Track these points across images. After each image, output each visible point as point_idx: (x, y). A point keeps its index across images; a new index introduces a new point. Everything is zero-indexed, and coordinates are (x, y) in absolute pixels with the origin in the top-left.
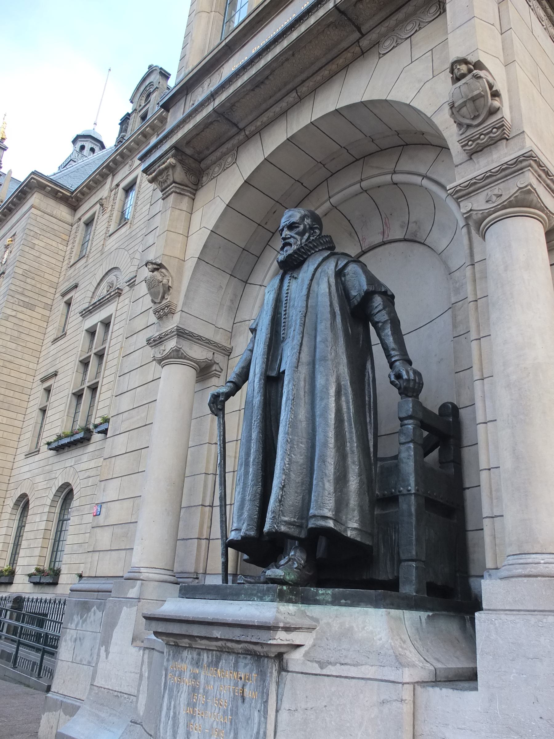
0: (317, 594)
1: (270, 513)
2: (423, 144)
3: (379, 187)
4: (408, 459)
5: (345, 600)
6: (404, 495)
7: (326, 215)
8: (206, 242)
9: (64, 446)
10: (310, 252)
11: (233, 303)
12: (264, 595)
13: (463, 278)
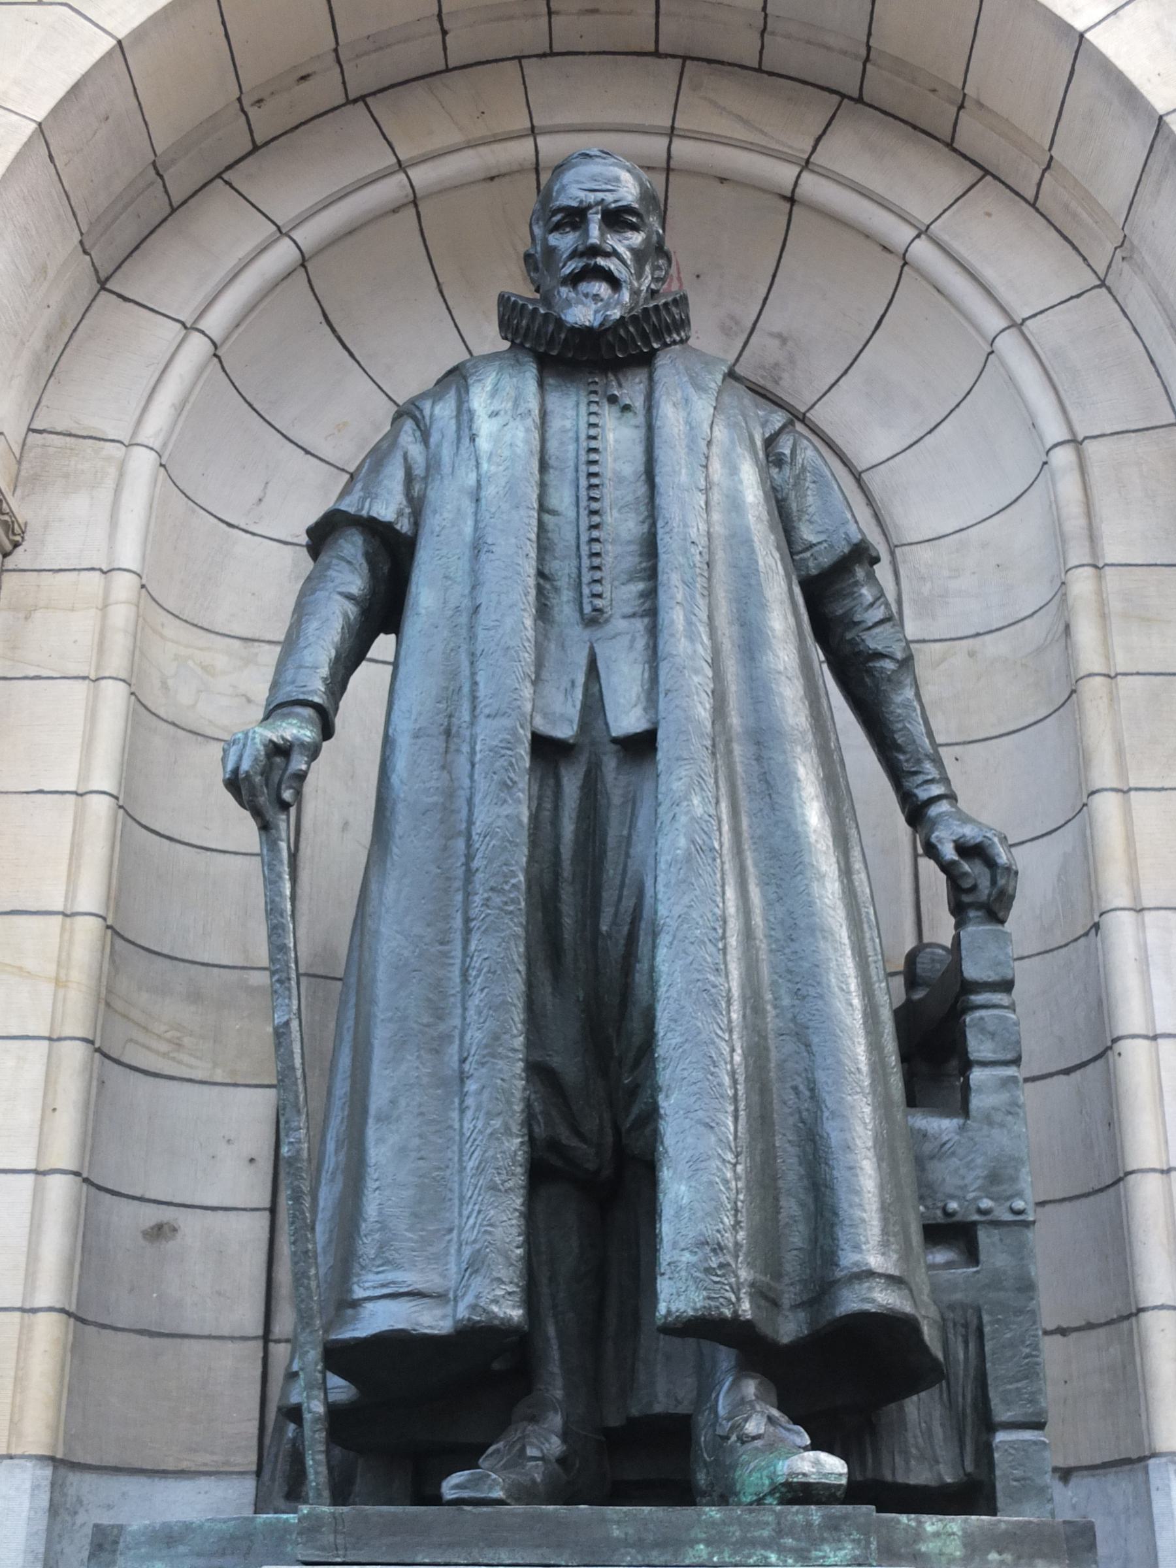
0: (918, 1535)
1: (286, 1226)
2: (915, 127)
3: (723, 180)
4: (1010, 1113)
5: (1000, 1553)
6: (997, 1224)
7: (492, 179)
8: (86, 76)
9: (492, 889)
10: (670, 334)
11: (47, 350)
12: (817, 1542)
13: (946, 573)
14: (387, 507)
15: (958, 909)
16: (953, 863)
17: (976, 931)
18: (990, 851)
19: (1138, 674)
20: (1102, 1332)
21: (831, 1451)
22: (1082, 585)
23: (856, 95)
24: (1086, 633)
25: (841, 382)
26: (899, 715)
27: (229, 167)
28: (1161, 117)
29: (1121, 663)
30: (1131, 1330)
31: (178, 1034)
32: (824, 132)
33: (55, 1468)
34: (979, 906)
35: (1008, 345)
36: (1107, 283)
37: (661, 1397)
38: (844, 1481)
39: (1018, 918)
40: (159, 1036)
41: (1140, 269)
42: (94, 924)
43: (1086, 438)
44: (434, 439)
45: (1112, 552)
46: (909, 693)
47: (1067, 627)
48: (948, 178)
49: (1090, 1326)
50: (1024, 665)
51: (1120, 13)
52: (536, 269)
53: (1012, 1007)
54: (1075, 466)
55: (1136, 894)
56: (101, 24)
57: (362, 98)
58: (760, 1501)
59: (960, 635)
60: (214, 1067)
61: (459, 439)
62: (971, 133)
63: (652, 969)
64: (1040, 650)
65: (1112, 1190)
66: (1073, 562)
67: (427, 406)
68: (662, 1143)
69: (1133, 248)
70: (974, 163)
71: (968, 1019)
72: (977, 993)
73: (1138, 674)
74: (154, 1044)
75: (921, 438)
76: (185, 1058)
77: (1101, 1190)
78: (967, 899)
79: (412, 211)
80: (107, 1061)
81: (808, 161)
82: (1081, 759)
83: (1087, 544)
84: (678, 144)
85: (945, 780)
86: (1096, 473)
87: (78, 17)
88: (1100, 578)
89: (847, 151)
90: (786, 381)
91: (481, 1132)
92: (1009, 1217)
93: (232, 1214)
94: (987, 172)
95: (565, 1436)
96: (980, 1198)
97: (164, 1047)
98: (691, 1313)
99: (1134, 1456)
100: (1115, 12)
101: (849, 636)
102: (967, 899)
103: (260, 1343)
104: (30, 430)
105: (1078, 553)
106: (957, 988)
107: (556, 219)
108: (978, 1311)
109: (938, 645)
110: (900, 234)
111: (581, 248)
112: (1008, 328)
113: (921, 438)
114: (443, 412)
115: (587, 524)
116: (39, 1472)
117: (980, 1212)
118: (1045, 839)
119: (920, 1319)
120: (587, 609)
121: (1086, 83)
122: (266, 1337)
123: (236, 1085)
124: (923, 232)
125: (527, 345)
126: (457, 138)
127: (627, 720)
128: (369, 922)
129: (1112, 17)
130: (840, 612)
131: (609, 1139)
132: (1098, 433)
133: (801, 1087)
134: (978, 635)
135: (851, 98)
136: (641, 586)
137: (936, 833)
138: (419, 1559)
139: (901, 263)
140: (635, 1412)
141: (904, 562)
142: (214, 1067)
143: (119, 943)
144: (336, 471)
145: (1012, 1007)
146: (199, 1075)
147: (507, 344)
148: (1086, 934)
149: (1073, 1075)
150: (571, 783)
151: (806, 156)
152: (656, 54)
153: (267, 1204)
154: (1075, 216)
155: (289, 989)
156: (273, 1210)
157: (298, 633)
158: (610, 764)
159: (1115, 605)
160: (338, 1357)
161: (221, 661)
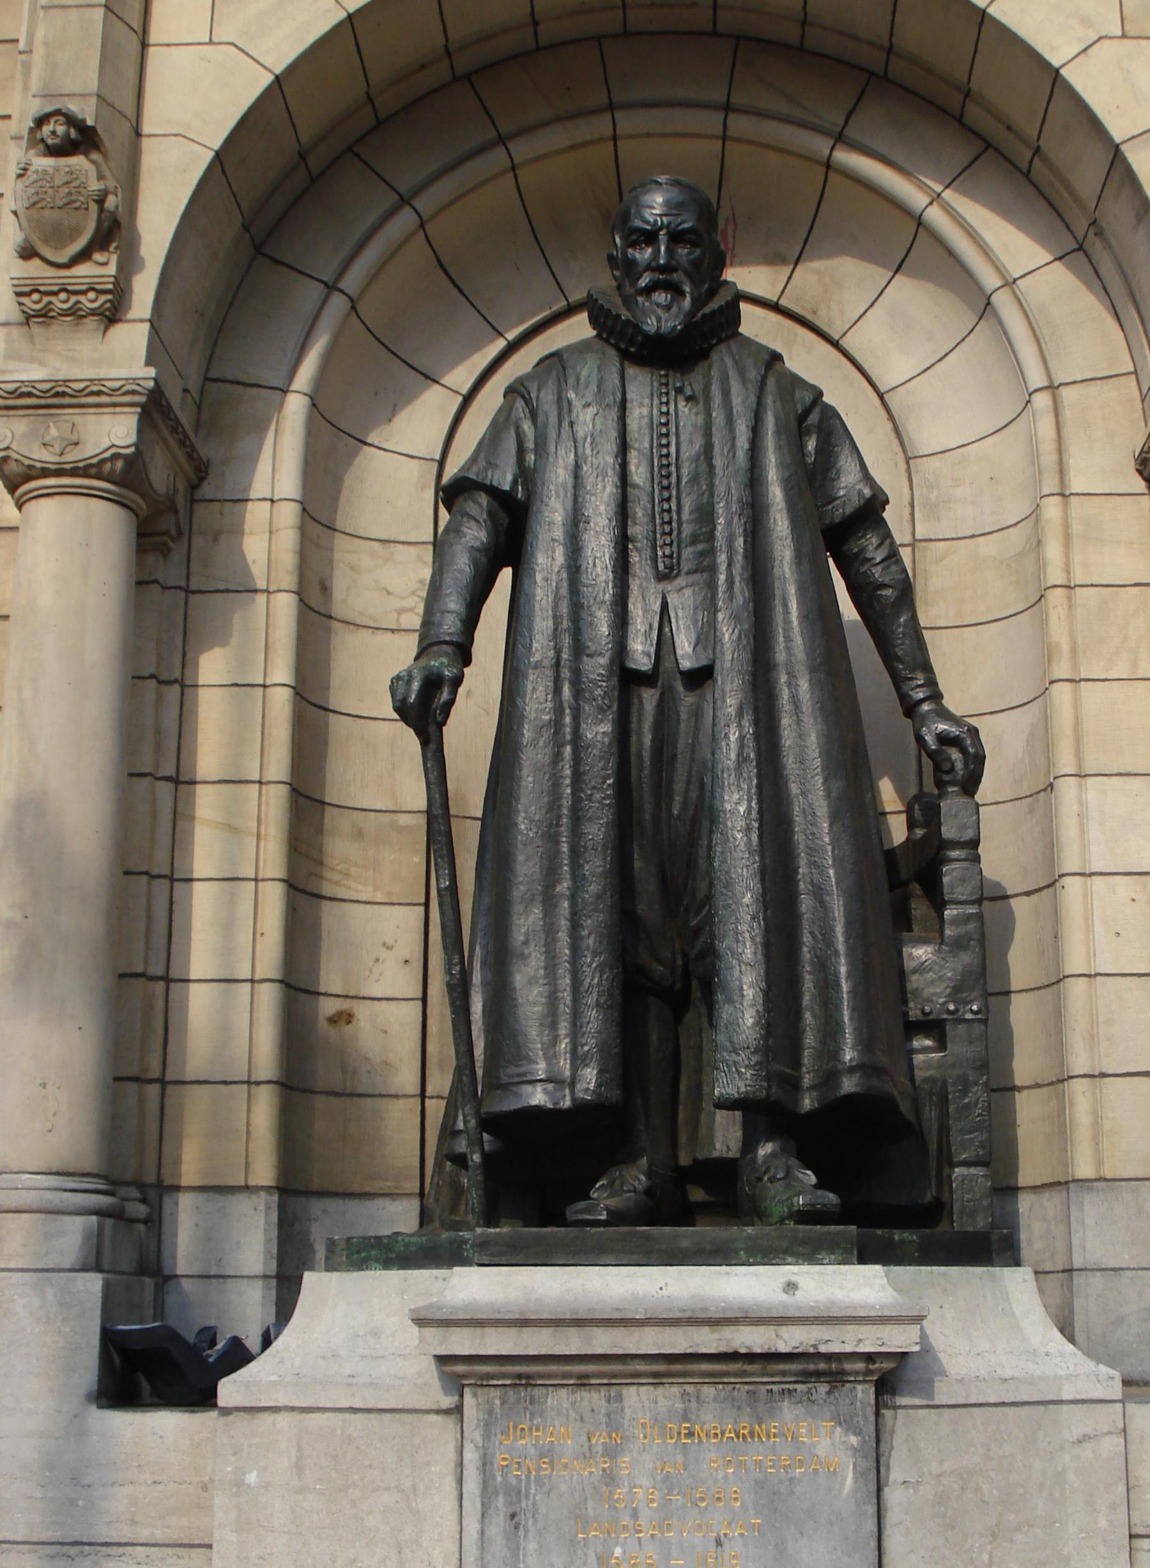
14: (504, 479)
19: (1092, 585)
20: (1045, 1089)
21: (831, 1191)
22: (1052, 509)
23: (882, 73)
24: (1053, 551)
25: (868, 313)
27: (358, 141)
28: (1117, 146)
29: (1079, 578)
30: (1064, 1091)
32: (855, 107)
33: (280, 1195)
36: (1086, 246)
37: (718, 1146)
38: (838, 1210)
39: (986, 790)
41: (1108, 245)
42: (283, 790)
43: (1060, 385)
44: (541, 418)
45: (1077, 484)
47: (1039, 542)
49: (1038, 1086)
50: (1009, 566)
51: (1089, 51)
54: (1051, 409)
55: (1080, 764)
56: (261, 61)
57: (467, 77)
58: (782, 1221)
59: (959, 535)
61: (560, 425)
62: (974, 114)
63: (710, 847)
64: (1021, 555)
65: (1055, 987)
66: (1046, 491)
67: (533, 388)
70: (978, 136)
72: (954, 849)
73: (1092, 585)
75: (933, 365)
77: (1048, 986)
78: (946, 778)
79: (511, 174)
80: (297, 893)
81: (841, 134)
82: (1048, 654)
83: (1057, 476)
84: (733, 118)
86: (1068, 413)
87: (242, 55)
88: (1066, 506)
90: (823, 313)
93: (394, 1003)
95: (649, 1174)
98: (736, 1096)
99: (1063, 1180)
100: (1085, 50)
101: (863, 570)
102: (946, 778)
103: (419, 1100)
104: (207, 379)
105: (1050, 484)
107: (634, 237)
108: (944, 1082)
109: (942, 544)
111: (654, 264)
112: (1002, 287)
113: (933, 365)
114: (546, 398)
116: (269, 1198)
117: (949, 1012)
118: (1019, 709)
119: (898, 1098)
120: (661, 567)
121: (1059, 106)
122: (423, 1095)
123: (392, 904)
125: (612, 341)
129: (1083, 55)
131: (679, 962)
132: (1071, 380)
134: (973, 536)
135: (878, 76)
138: (553, 1262)
140: (700, 1156)
141: (917, 472)
143: (302, 800)
144: (451, 393)
146: (364, 897)
147: (595, 333)
148: (1045, 790)
149: (1032, 897)
150: (649, 698)
151: (839, 130)
152: (714, 33)
153: (420, 995)
156: (424, 1000)
157: (441, 579)
158: (680, 687)
159: (1077, 528)
160: (490, 1123)
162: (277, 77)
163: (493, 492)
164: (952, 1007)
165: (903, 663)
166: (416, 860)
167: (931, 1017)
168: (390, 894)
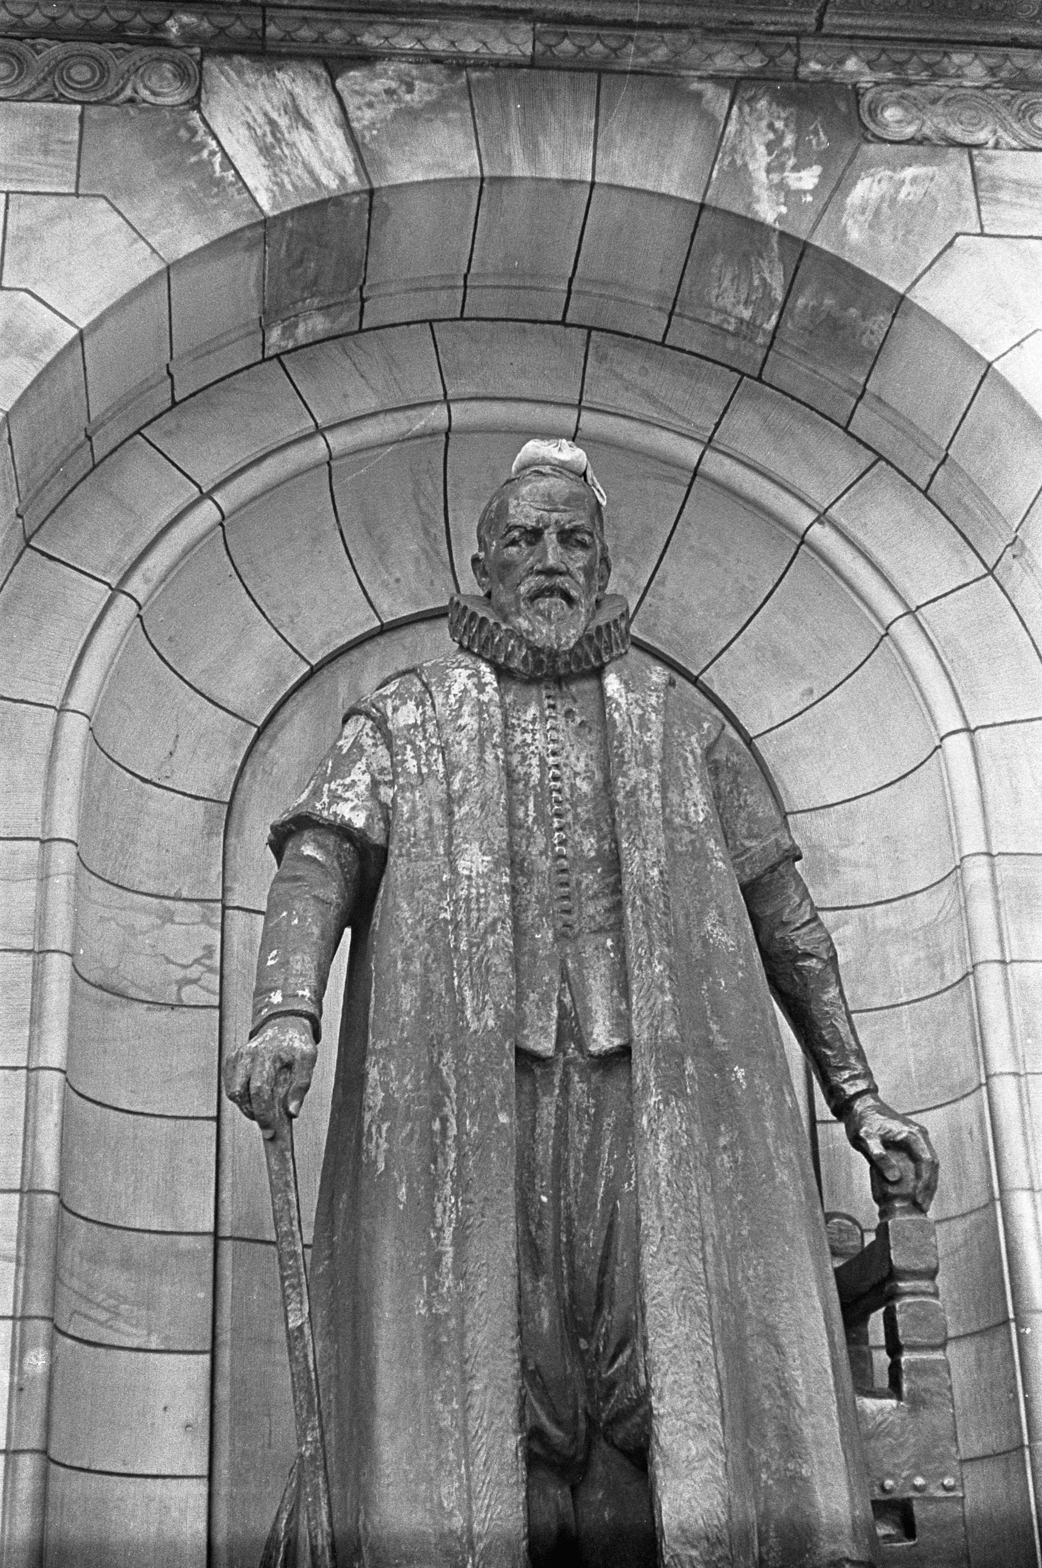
15: (883, 1198)
16: (882, 1158)
17: (901, 1220)
18: (914, 1146)
26: (827, 1013)
31: (115, 1303)
34: (903, 1197)
35: (904, 629)
40: (98, 1305)
43: (977, 728)
46: (833, 992)
48: (846, 463)
52: (485, 573)
53: (936, 1294)
60: (149, 1334)
62: (864, 422)
68: (657, 1442)
69: (1023, 547)
71: (897, 1305)
74: (92, 1313)
76: (121, 1325)
78: (892, 1190)
85: (868, 1075)
89: (745, 425)
91: (485, 1430)
92: (941, 1493)
94: (881, 457)
96: (915, 1475)
97: (103, 1316)
101: (778, 935)
106: (885, 1274)
110: (803, 517)
111: (539, 567)
115: (939, 1279)
117: (916, 1488)
124: (822, 517)
126: (371, 403)
127: (602, 1037)
128: (364, 1223)
130: (769, 912)
133: (773, 1386)
136: (605, 902)
137: (864, 1129)
139: (798, 542)
142: (149, 1334)
145: (936, 1294)
151: (709, 434)
154: (967, 510)
155: (300, 1294)
156: (210, 1477)
161: (144, 921)
162: (81, 331)
163: (344, 831)
164: (919, 1481)
165: (831, 1048)
166: (201, 1295)
167: (893, 1496)
168: (167, 1338)
